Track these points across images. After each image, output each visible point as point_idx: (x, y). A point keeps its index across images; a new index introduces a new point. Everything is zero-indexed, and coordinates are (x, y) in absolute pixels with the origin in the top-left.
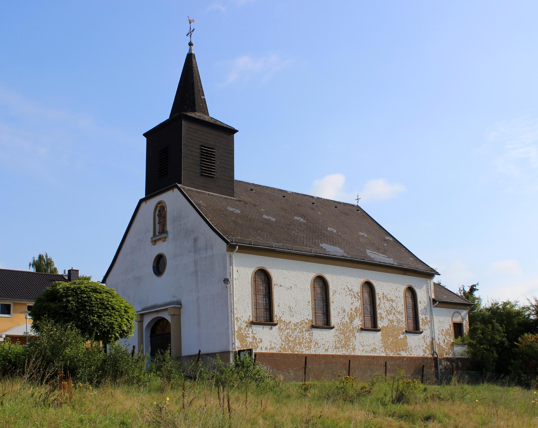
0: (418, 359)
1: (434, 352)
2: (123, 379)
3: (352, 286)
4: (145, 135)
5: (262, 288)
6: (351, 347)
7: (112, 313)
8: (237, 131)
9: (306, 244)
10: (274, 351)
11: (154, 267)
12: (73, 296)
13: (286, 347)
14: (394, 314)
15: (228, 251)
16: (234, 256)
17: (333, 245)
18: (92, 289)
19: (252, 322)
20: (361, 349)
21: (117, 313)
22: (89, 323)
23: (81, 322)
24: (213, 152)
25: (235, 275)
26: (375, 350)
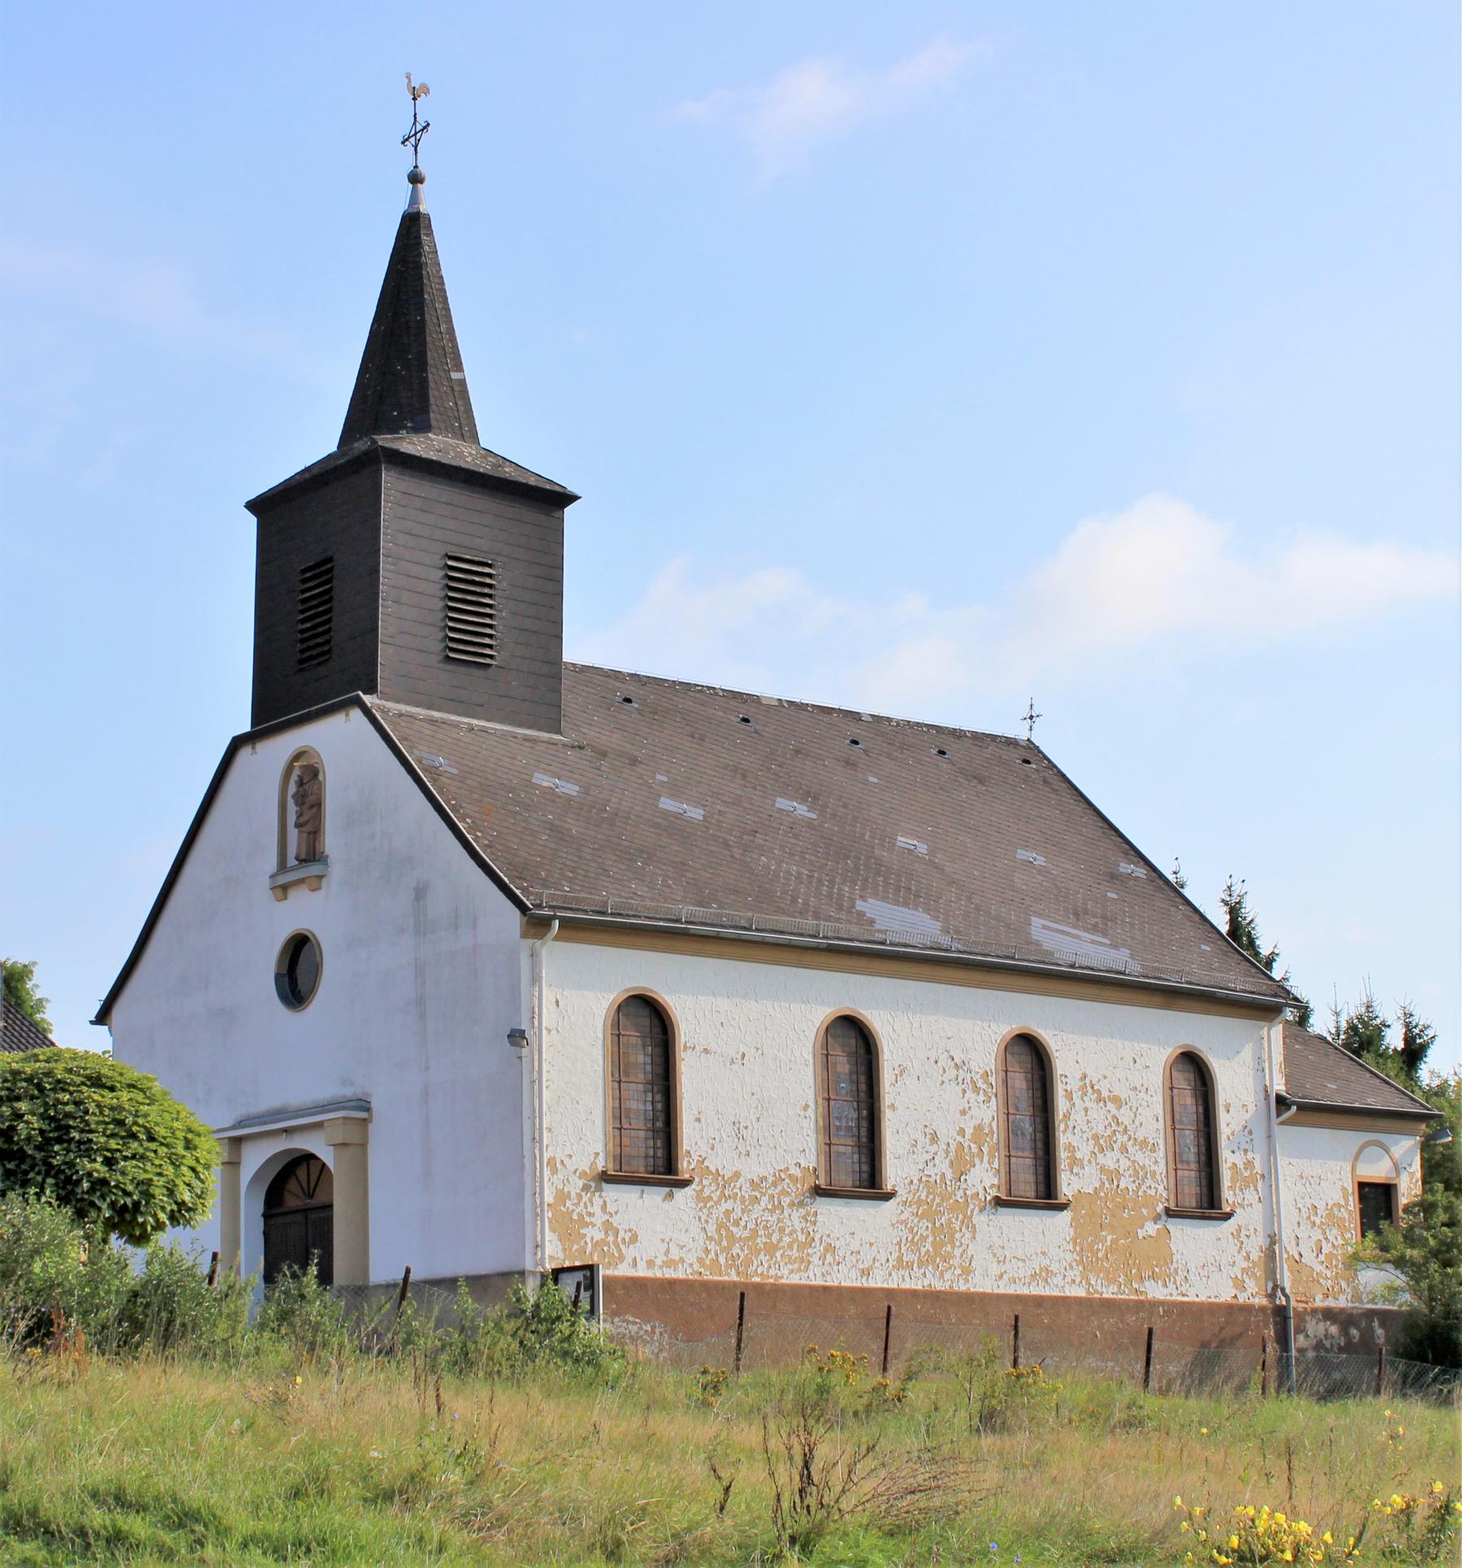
0: (1212, 1309)
1: (1275, 1287)
2: (184, 1347)
3: (965, 1050)
5: (641, 1059)
6: (955, 1262)
7: (147, 1149)
8: (571, 498)
9: (806, 904)
10: (680, 1274)
11: (278, 977)
12: (32, 1098)
13: (722, 1260)
14: (1124, 1150)
15: (524, 935)
16: (544, 953)
17: (906, 904)
18: (89, 1078)
19: (604, 1173)
20: (995, 1269)
21: (162, 1151)
22: (79, 1182)
23: (55, 1177)
24: (490, 576)
25: (548, 1017)
26: (1045, 1274)
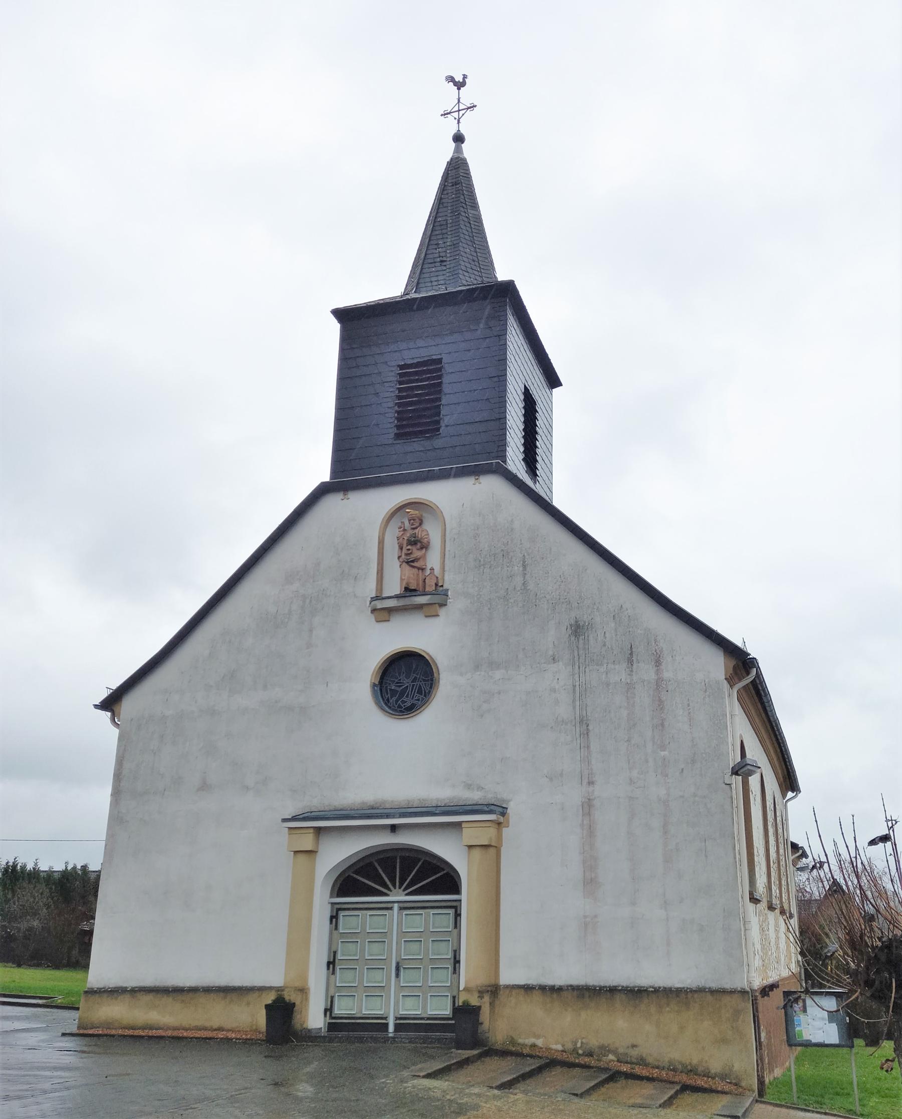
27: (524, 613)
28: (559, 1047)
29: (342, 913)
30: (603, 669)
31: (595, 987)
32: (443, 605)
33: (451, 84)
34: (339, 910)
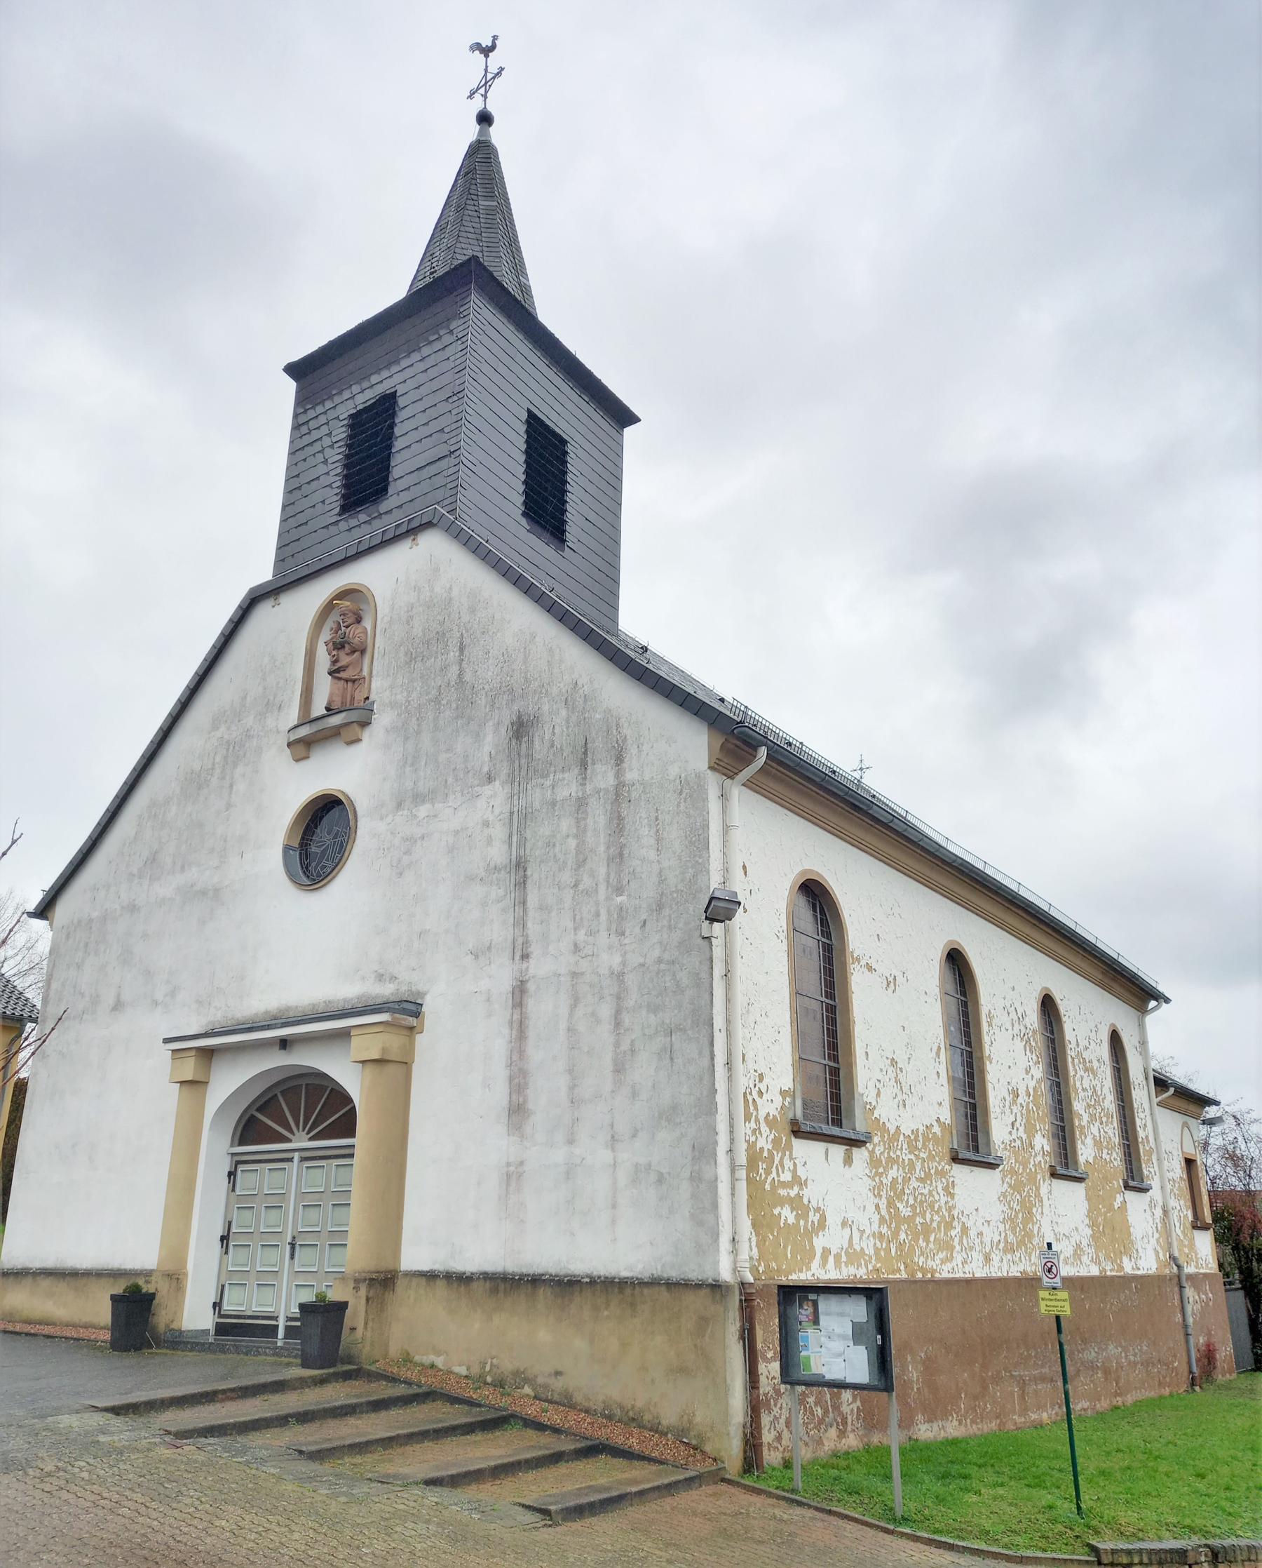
4: (296, 370)
8: (638, 420)
27: (457, 718)
28: (463, 1371)
29: (241, 1168)
30: (548, 783)
31: (514, 1274)
32: (365, 724)
33: (477, 52)
34: (238, 1163)
